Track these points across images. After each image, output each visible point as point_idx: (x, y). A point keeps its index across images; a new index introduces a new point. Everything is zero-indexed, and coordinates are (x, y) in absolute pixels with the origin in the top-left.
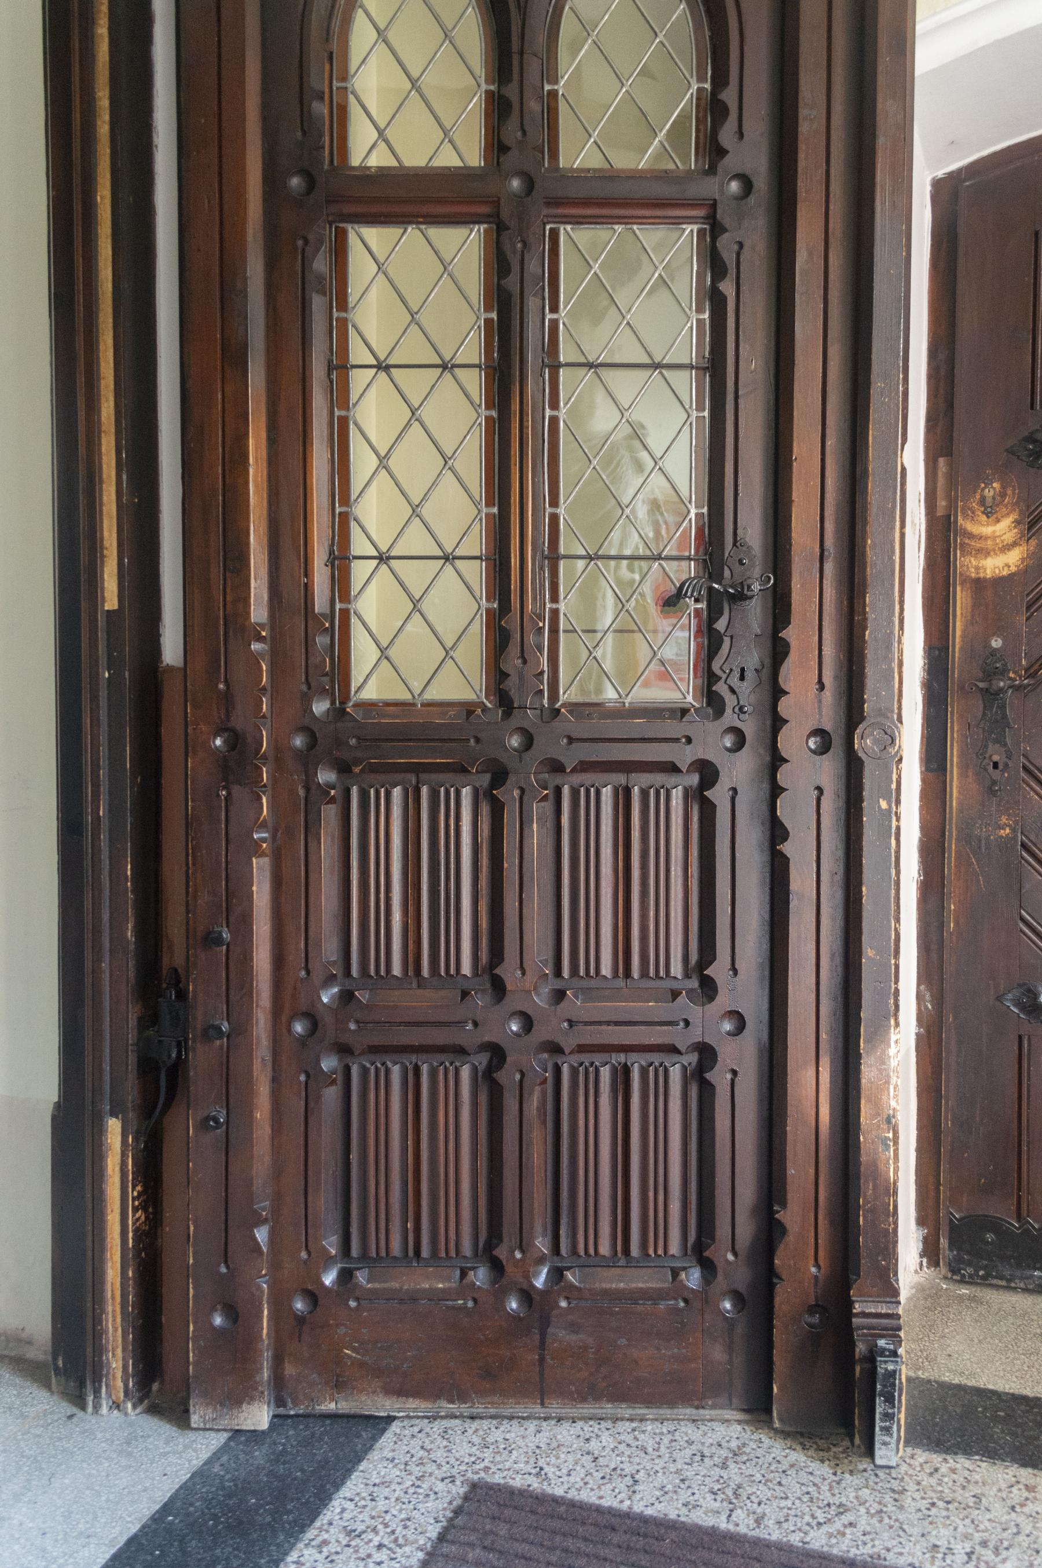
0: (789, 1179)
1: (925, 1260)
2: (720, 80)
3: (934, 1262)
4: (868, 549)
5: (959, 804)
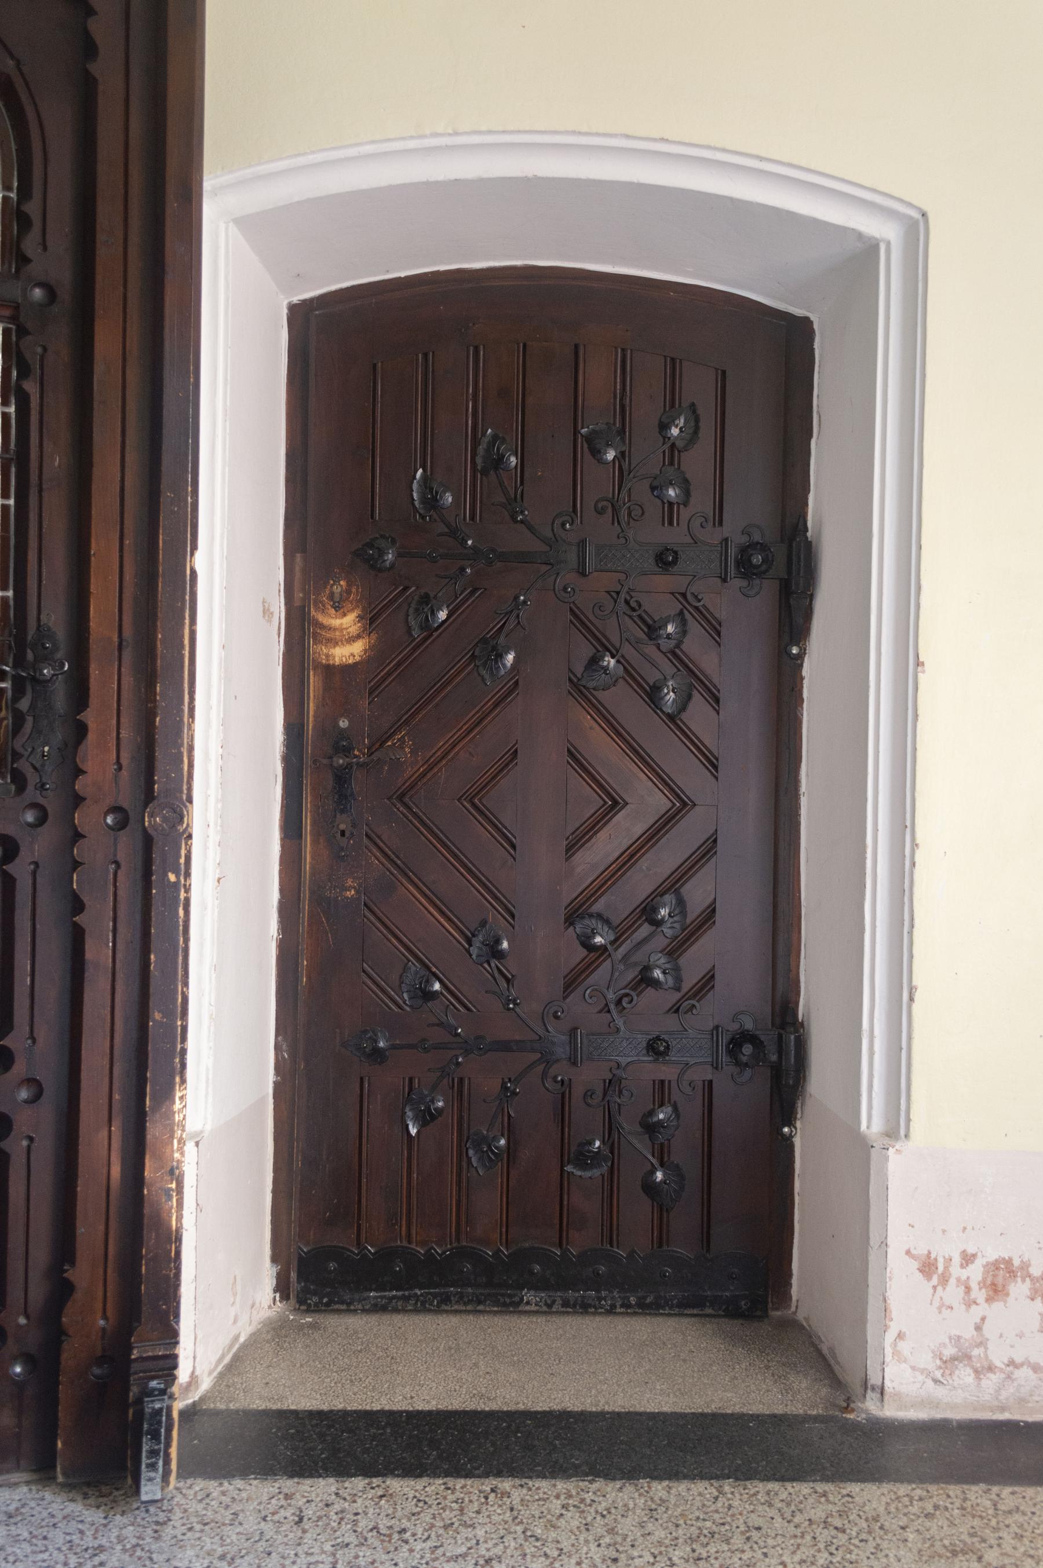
0: (79, 1239)
1: (278, 1295)
2: (25, 192)
3: (285, 1297)
4: (159, 643)
5: (312, 867)
